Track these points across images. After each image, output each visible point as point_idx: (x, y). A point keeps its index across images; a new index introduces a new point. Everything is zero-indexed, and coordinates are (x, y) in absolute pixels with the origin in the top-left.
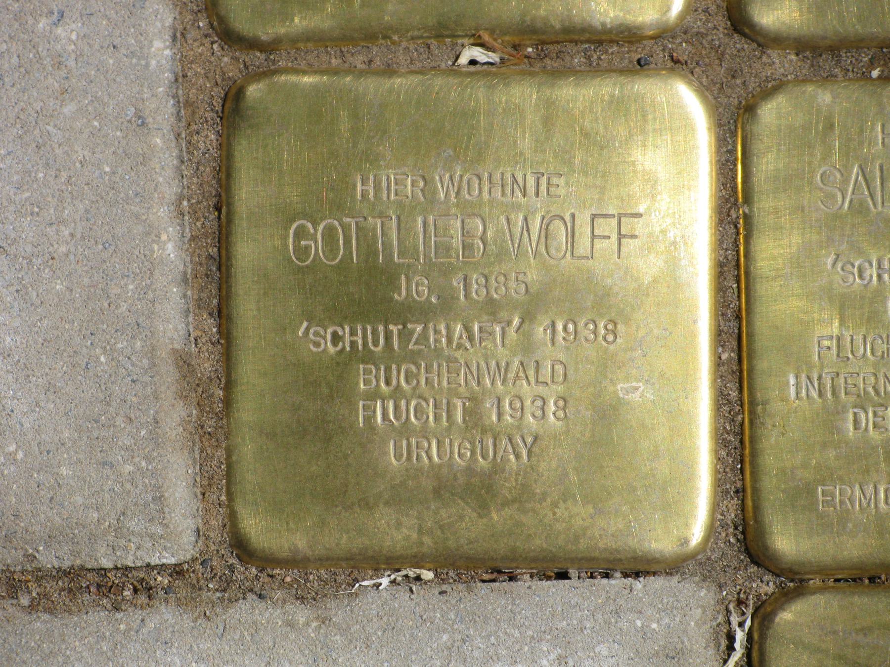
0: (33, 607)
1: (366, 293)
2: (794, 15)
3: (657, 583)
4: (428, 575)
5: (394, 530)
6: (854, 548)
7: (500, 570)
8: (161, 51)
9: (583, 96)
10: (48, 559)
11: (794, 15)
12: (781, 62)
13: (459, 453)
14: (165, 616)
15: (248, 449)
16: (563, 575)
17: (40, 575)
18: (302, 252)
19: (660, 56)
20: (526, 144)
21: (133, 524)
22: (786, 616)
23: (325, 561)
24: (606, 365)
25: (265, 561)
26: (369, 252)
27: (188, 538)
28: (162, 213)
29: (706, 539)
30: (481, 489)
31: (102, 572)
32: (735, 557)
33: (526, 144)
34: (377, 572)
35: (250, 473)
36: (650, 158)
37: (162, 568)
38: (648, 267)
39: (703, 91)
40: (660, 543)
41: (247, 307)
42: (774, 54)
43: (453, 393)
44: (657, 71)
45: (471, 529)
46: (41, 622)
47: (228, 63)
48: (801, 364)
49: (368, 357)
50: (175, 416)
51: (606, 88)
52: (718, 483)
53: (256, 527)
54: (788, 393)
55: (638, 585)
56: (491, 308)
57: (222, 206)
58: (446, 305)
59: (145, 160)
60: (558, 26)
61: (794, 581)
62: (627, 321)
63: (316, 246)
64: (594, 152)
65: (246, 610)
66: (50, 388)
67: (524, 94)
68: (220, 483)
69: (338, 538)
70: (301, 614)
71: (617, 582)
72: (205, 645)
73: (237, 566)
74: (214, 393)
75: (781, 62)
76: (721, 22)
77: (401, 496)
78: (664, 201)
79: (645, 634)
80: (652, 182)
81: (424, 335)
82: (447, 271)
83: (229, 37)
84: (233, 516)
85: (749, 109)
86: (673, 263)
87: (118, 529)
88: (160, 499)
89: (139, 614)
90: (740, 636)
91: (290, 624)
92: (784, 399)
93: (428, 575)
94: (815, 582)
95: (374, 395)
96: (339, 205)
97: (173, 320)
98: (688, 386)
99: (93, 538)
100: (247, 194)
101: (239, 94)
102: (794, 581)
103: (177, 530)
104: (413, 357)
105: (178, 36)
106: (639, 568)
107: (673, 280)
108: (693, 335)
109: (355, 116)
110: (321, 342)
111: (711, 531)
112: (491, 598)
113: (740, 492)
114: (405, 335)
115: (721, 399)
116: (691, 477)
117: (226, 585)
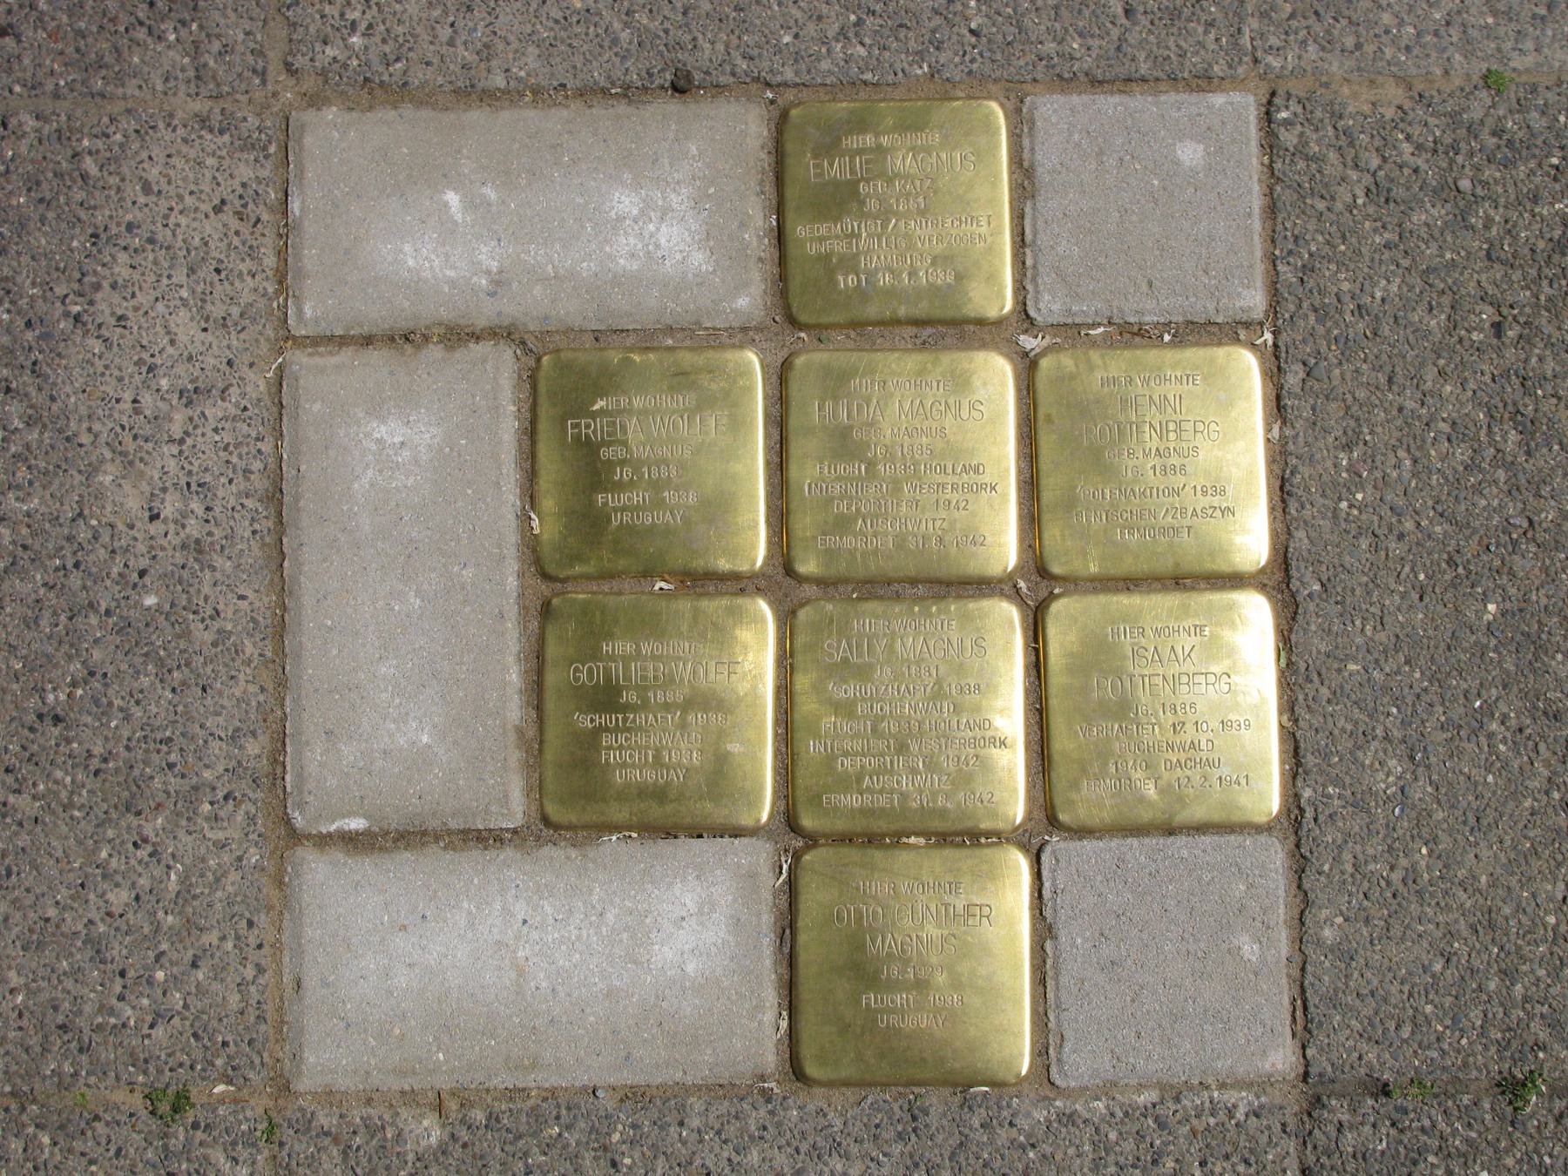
0: (446, 848)
1: (606, 698)
2: (694, 150)
3: (745, 840)
4: (634, 835)
5: (619, 814)
6: (840, 825)
7: (670, 833)
8: (512, 582)
9: (713, 606)
10: (453, 824)
11: (694, 150)
12: (810, 590)
13: (650, 776)
14: (509, 853)
15: (549, 773)
16: (700, 836)
17: (450, 832)
18: (577, 679)
19: (751, 587)
20: (685, 628)
21: (493, 808)
22: (807, 857)
23: (585, 827)
24: (722, 734)
25: (557, 827)
26: (608, 678)
27: (520, 815)
28: (511, 659)
29: (769, 819)
30: (659, 794)
31: (479, 831)
32: (783, 828)
33: (685, 628)
34: (611, 833)
35: (551, 785)
36: (745, 635)
37: (507, 830)
38: (743, 688)
39: (770, 603)
40: (746, 821)
41: (550, 705)
42: (806, 586)
43: (647, 747)
44: (749, 595)
45: (655, 812)
46: (449, 855)
47: (544, 588)
48: (816, 735)
49: (607, 729)
50: (515, 757)
51: (725, 602)
52: (775, 793)
53: (551, 810)
54: (812, 749)
55: (737, 841)
56: (667, 707)
57: (540, 656)
58: (644, 706)
59: (503, 634)
60: (973, 1032)
61: (812, 841)
62: (732, 713)
63: (584, 676)
64: (719, 636)
65: (547, 850)
66: (455, 743)
67: (684, 605)
68: (537, 789)
69: (591, 817)
70: (574, 853)
71: (726, 840)
72: (527, 868)
73: (546, 828)
74: (534, 746)
75: (810, 590)
76: (781, 570)
77: (622, 796)
78: (751, 657)
79: (738, 865)
80: (745, 647)
81: (634, 720)
82: (646, 689)
83: (545, 576)
84: (542, 805)
85: (794, 612)
86: (754, 688)
87: (486, 811)
88: (506, 796)
89: (495, 853)
90: (785, 867)
91: (568, 858)
92: (808, 752)
93: (634, 835)
94: (822, 841)
95: (610, 748)
96: (595, 655)
97: (515, 710)
98: (762, 742)
99: (474, 815)
100: (552, 651)
101: (549, 603)
102: (812, 841)
103: (515, 810)
104: (628, 730)
105: (521, 575)
106: (737, 832)
107: (755, 695)
108: (764, 721)
109: (603, 613)
110: (585, 722)
111: (771, 816)
112: (666, 847)
113: (786, 797)
114: (625, 719)
115: (777, 752)
116: (762, 788)
117: (538, 838)
